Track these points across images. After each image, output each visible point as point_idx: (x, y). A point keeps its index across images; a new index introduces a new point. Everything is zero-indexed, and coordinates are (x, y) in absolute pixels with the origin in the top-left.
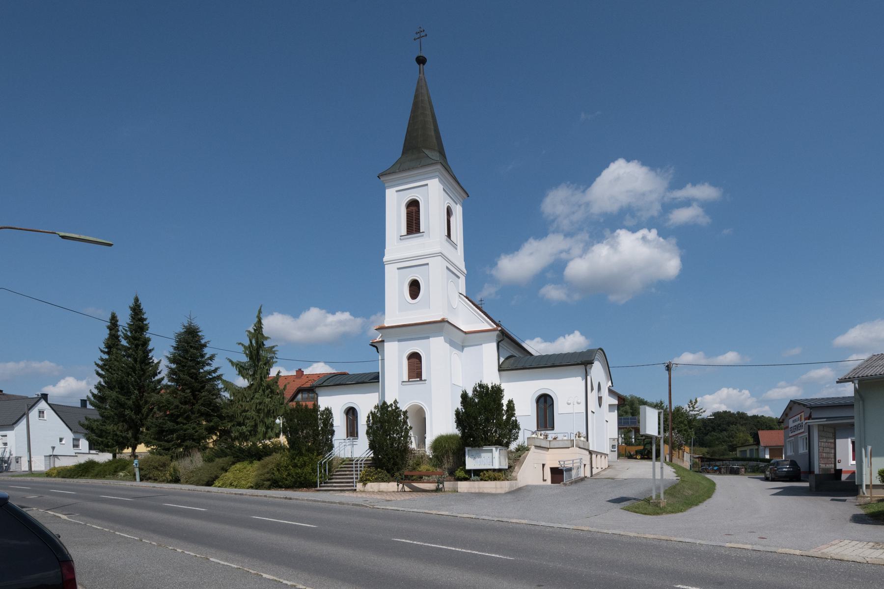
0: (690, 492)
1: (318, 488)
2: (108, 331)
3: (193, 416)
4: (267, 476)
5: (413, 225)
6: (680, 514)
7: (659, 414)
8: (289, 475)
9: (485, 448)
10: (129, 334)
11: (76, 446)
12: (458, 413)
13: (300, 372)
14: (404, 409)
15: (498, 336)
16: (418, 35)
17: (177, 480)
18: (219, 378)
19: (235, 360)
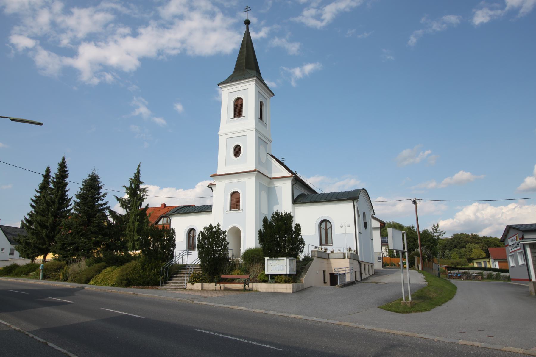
0: (435, 295)
2: (43, 179)
4: (125, 277)
5: (238, 111)
6: (426, 313)
7: (403, 234)
10: (55, 180)
11: (11, 254)
12: (260, 232)
14: (224, 230)
15: (292, 180)
17: (66, 279)
18: (108, 208)
19: (119, 197)
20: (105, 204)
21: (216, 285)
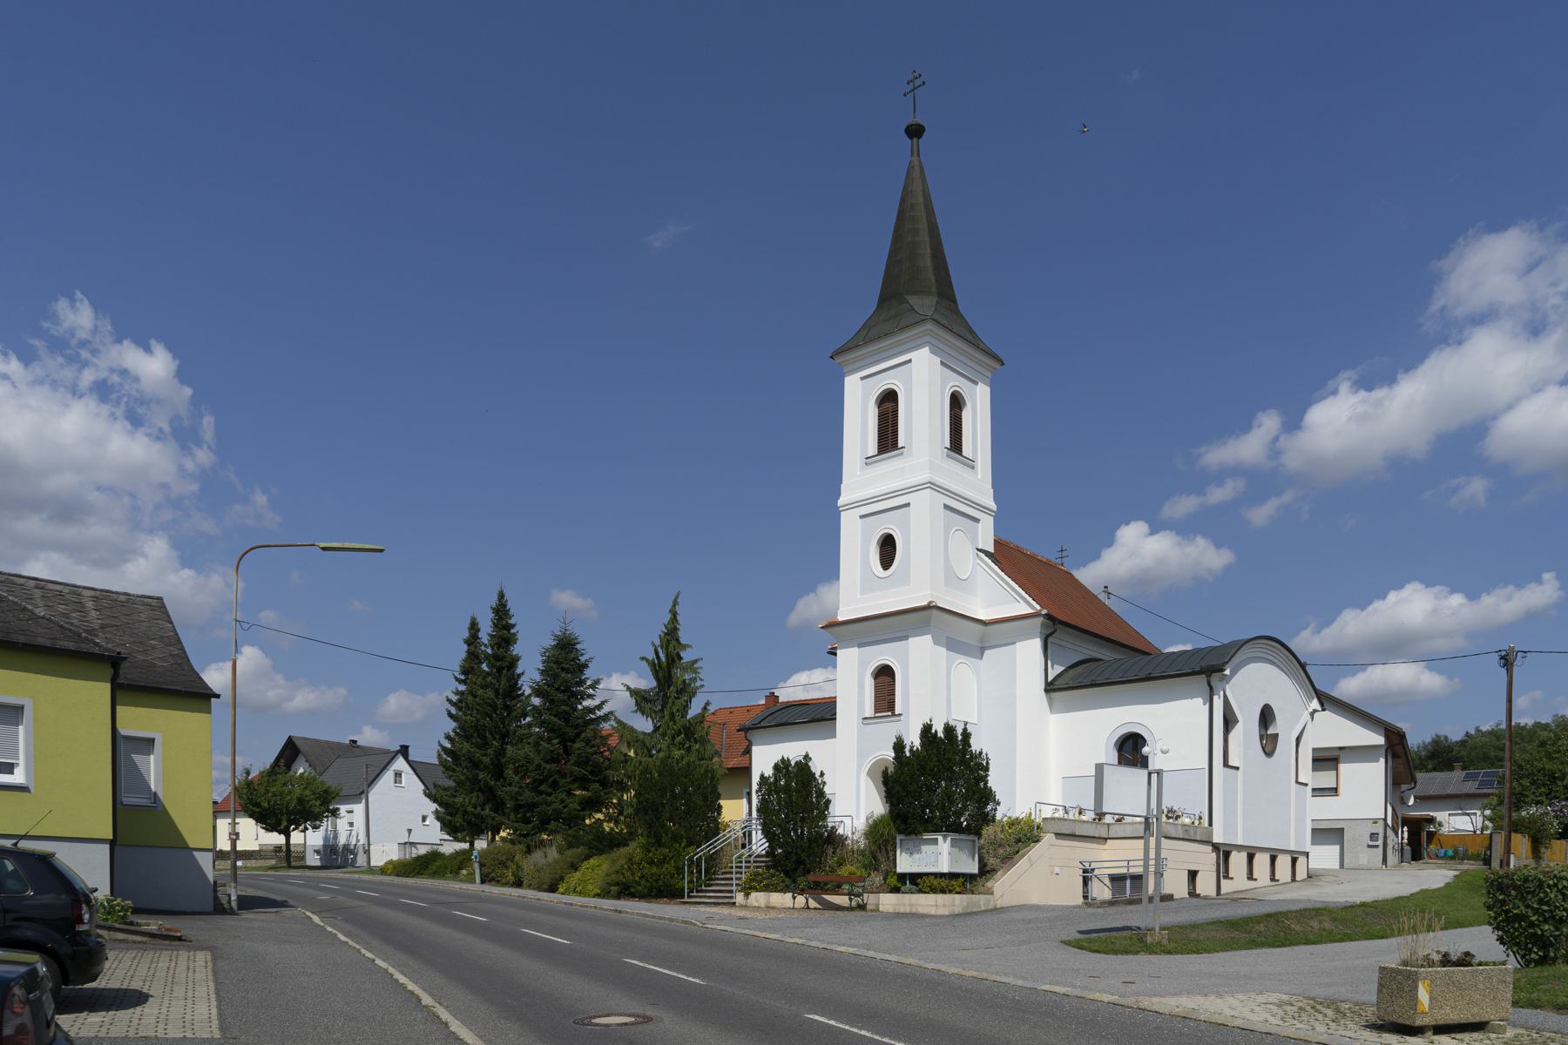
2: (465, 647)
3: (562, 782)
4: (614, 877)
5: (888, 439)
8: (642, 877)
9: (927, 836)
13: (772, 698)
16: (911, 86)
17: (518, 884)
20: (599, 707)
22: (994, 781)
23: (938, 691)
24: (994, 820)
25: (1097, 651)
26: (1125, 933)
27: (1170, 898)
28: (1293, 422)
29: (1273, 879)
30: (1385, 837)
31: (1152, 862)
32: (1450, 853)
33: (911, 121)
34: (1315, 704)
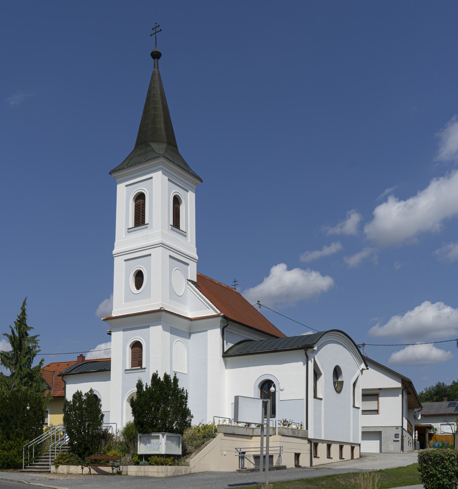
1: (23, 470)
5: (140, 219)
9: (154, 434)
13: (82, 357)
15: (222, 321)
16: (154, 31)
21: (83, 468)
22: (191, 405)
23: (165, 356)
24: (190, 426)
25: (251, 335)
26: (251, 486)
27: (284, 468)
28: (368, 216)
29: (341, 457)
30: (402, 436)
31: (265, 449)
32: (440, 445)
33: (154, 49)
34: (363, 366)
